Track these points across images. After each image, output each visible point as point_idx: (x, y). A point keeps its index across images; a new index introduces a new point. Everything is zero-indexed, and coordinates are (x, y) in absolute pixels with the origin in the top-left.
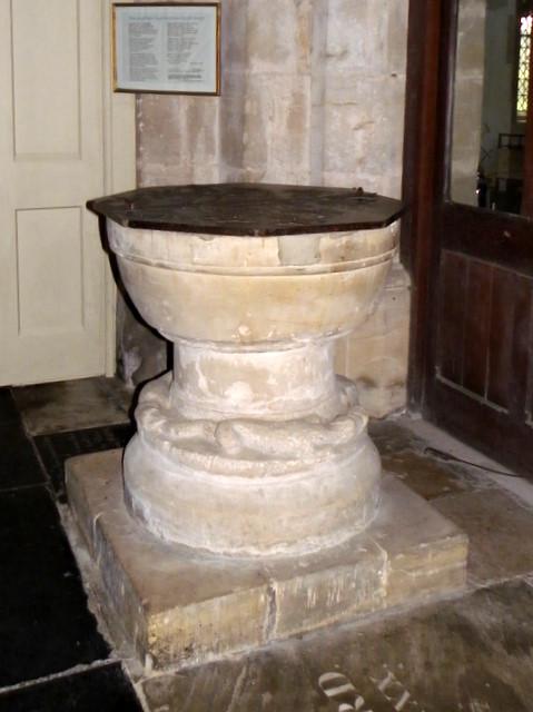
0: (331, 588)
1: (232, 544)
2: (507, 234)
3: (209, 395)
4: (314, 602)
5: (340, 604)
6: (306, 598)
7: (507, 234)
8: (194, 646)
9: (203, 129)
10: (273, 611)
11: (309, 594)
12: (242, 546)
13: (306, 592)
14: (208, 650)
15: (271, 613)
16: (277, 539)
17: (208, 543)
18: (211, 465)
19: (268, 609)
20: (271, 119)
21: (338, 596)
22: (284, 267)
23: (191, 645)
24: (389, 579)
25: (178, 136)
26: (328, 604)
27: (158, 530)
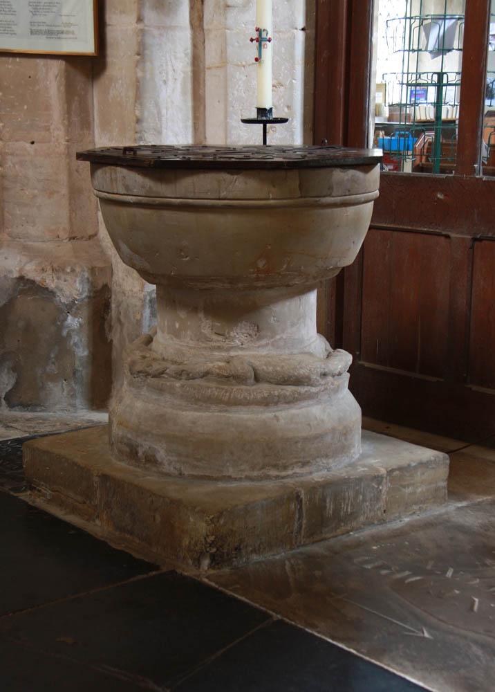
0: (344, 499)
1: (253, 468)
2: (440, 196)
3: (215, 337)
4: (331, 512)
5: (351, 513)
6: (325, 507)
7: (440, 196)
8: (242, 547)
9: (76, 98)
10: (300, 517)
11: (328, 505)
12: (263, 468)
13: (325, 501)
14: (252, 551)
15: (299, 519)
16: (295, 460)
17: (231, 469)
18: (229, 398)
19: (297, 516)
20: (165, 82)
21: (349, 507)
22: (303, 199)
23: (240, 545)
24: (388, 493)
25: (48, 108)
26: (342, 513)
27: (175, 468)
